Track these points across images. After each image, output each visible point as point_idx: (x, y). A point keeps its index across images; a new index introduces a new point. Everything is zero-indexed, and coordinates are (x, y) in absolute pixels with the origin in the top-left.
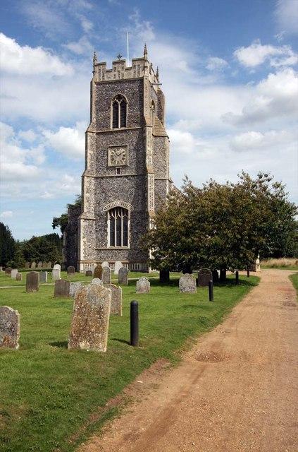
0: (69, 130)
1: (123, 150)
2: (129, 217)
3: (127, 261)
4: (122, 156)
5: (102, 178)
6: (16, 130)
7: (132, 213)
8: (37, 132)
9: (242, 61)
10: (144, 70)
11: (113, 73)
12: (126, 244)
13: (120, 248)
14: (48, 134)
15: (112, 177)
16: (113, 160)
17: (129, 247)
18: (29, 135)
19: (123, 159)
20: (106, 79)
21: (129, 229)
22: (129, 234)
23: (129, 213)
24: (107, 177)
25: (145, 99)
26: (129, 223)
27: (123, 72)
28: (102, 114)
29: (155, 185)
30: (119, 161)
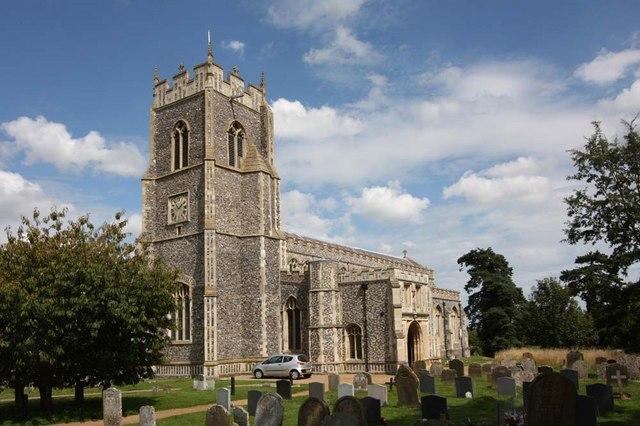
0: (381, 190)
1: (184, 199)
2: (191, 296)
3: (189, 362)
4: (182, 208)
5: (162, 242)
6: (317, 198)
7: (194, 290)
8: (339, 199)
9: (590, 81)
10: (207, 79)
11: (173, 93)
12: (188, 338)
13: (181, 342)
14: (350, 200)
15: (171, 240)
16: (173, 215)
17: (191, 341)
18: (330, 203)
19: (184, 212)
20: (167, 103)
21: (191, 315)
22: (191, 321)
23: (190, 290)
24: (166, 241)
25: (207, 121)
26: (191, 304)
27: (183, 88)
28: (162, 153)
29: (277, 254)
30: (180, 217)
